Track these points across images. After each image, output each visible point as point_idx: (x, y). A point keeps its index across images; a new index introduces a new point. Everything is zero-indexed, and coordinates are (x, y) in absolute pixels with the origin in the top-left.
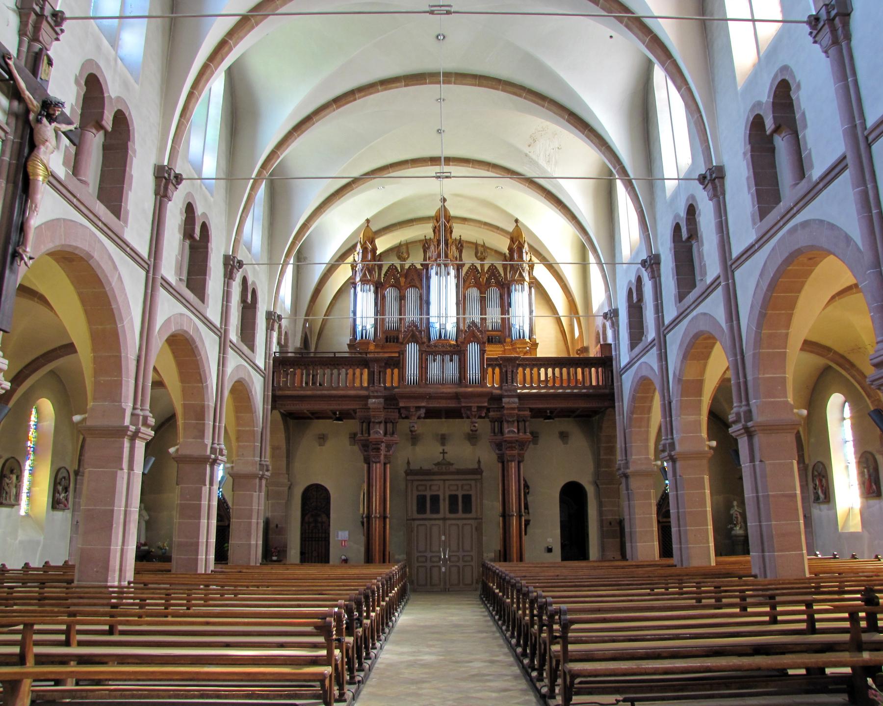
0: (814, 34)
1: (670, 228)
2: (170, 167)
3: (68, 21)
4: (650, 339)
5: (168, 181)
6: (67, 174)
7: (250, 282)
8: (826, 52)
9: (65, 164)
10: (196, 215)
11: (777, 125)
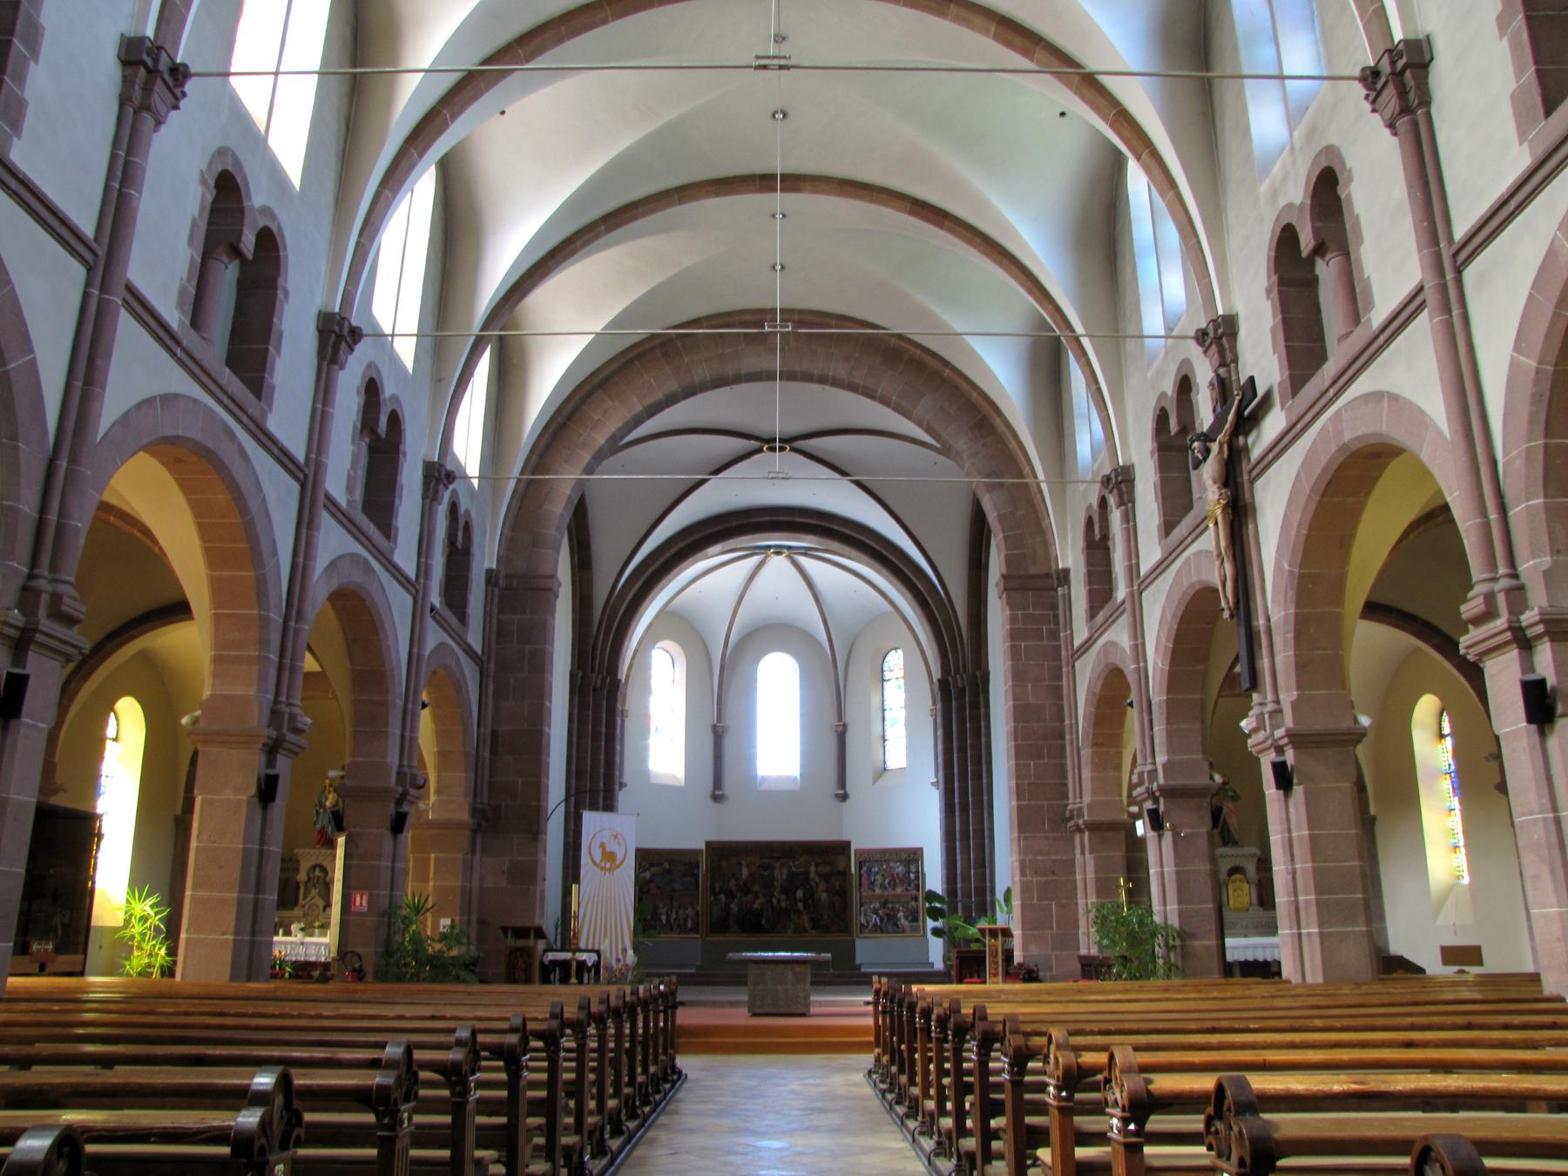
0: (1371, 97)
1: (1151, 417)
2: (343, 315)
3: (194, 78)
5: (340, 337)
6: (181, 323)
7: (462, 510)
8: (1391, 126)
9: (181, 305)
10: (382, 398)
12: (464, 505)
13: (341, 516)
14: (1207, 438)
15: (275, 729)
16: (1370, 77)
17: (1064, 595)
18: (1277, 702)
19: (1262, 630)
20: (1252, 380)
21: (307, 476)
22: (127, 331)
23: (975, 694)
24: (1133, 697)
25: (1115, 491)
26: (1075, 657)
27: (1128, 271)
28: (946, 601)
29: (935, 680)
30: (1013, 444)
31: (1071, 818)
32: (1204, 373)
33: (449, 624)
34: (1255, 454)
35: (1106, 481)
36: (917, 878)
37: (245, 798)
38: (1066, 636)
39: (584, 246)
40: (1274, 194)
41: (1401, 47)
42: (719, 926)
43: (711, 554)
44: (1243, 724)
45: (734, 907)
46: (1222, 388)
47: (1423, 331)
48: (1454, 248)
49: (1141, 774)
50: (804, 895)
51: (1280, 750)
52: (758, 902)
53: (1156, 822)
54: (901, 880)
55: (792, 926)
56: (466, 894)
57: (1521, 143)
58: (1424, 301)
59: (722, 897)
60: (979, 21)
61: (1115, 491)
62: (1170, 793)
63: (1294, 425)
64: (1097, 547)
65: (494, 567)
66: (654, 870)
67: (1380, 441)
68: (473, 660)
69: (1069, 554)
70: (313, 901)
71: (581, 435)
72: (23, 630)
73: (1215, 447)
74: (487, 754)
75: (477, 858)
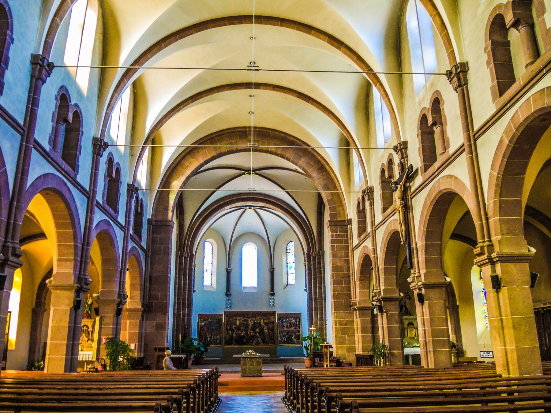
2: (101, 138)
3: (55, 68)
4: (368, 232)
5: (100, 146)
6: (50, 149)
8: (456, 89)
11: (517, 19)
12: (140, 197)
13: (100, 207)
14: (396, 183)
15: (79, 284)
16: (449, 74)
17: (350, 228)
18: (419, 273)
19: (414, 248)
20: (411, 165)
21: (90, 195)
22: (35, 155)
23: (320, 259)
24: (373, 266)
25: (367, 195)
26: (354, 249)
27: (372, 107)
28: (309, 226)
29: (305, 254)
30: (332, 175)
31: (352, 306)
32: (397, 159)
33: (135, 240)
34: (413, 189)
35: (364, 192)
36: (299, 324)
37: (69, 308)
38: (351, 242)
39: (183, 107)
40: (420, 103)
41: (459, 65)
42: (229, 342)
43: (226, 209)
44: (408, 280)
45: (234, 335)
46: (402, 166)
47: (464, 158)
48: (474, 133)
49: (375, 293)
50: (259, 331)
51: (420, 289)
52: (243, 333)
53: (381, 309)
54: (294, 325)
55: (255, 342)
56: (140, 334)
57: (493, 103)
58: (464, 149)
59: (230, 332)
60: (322, 36)
61: (367, 195)
62: (385, 299)
63: (425, 182)
64: (361, 212)
65: (151, 218)
66: (205, 322)
67: (451, 191)
68: (143, 251)
69: (352, 213)
70: (84, 338)
71: (181, 171)
72: (4, 261)
73: (399, 186)
74: (148, 284)
75: (144, 321)
